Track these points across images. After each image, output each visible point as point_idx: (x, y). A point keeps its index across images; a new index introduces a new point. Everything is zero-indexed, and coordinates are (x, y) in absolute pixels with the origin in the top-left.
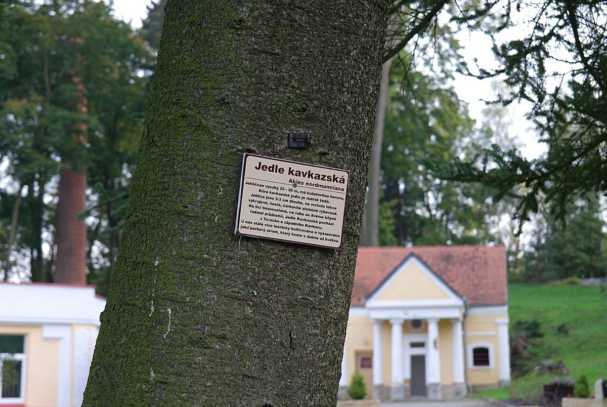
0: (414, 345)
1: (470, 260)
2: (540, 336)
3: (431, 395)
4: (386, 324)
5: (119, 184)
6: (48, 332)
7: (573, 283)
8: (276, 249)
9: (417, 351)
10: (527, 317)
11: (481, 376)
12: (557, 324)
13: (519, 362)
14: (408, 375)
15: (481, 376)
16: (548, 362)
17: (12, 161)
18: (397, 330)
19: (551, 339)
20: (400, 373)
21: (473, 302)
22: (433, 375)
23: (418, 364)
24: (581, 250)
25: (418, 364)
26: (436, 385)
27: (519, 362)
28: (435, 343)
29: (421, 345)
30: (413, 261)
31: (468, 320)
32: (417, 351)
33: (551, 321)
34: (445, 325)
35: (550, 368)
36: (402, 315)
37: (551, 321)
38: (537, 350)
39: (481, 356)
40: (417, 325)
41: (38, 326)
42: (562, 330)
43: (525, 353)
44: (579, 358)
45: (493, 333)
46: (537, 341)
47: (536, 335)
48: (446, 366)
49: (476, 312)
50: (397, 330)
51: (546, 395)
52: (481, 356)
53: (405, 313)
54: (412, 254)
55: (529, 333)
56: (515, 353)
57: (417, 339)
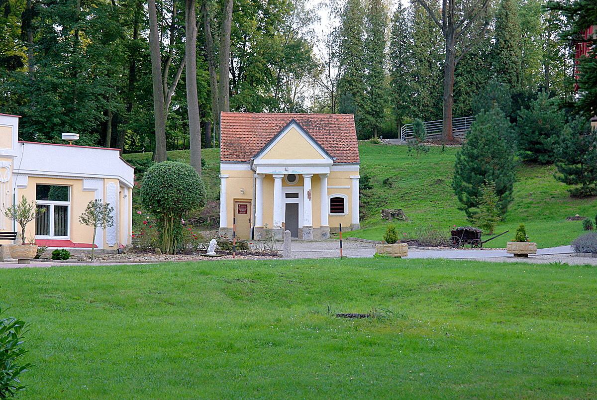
0: (288, 196)
2: (370, 188)
3: (305, 237)
6: (87, 184)
7: (375, 143)
11: (339, 219)
12: (381, 179)
18: (278, 183)
20: (279, 218)
22: (305, 219)
23: (292, 211)
24: (368, 113)
25: (292, 211)
28: (309, 194)
29: (296, 195)
30: (293, 126)
34: (317, 179)
38: (369, 200)
39: (337, 205)
40: (291, 178)
41: (80, 179)
50: (278, 183)
51: (453, 239)
52: (337, 205)
54: (293, 121)
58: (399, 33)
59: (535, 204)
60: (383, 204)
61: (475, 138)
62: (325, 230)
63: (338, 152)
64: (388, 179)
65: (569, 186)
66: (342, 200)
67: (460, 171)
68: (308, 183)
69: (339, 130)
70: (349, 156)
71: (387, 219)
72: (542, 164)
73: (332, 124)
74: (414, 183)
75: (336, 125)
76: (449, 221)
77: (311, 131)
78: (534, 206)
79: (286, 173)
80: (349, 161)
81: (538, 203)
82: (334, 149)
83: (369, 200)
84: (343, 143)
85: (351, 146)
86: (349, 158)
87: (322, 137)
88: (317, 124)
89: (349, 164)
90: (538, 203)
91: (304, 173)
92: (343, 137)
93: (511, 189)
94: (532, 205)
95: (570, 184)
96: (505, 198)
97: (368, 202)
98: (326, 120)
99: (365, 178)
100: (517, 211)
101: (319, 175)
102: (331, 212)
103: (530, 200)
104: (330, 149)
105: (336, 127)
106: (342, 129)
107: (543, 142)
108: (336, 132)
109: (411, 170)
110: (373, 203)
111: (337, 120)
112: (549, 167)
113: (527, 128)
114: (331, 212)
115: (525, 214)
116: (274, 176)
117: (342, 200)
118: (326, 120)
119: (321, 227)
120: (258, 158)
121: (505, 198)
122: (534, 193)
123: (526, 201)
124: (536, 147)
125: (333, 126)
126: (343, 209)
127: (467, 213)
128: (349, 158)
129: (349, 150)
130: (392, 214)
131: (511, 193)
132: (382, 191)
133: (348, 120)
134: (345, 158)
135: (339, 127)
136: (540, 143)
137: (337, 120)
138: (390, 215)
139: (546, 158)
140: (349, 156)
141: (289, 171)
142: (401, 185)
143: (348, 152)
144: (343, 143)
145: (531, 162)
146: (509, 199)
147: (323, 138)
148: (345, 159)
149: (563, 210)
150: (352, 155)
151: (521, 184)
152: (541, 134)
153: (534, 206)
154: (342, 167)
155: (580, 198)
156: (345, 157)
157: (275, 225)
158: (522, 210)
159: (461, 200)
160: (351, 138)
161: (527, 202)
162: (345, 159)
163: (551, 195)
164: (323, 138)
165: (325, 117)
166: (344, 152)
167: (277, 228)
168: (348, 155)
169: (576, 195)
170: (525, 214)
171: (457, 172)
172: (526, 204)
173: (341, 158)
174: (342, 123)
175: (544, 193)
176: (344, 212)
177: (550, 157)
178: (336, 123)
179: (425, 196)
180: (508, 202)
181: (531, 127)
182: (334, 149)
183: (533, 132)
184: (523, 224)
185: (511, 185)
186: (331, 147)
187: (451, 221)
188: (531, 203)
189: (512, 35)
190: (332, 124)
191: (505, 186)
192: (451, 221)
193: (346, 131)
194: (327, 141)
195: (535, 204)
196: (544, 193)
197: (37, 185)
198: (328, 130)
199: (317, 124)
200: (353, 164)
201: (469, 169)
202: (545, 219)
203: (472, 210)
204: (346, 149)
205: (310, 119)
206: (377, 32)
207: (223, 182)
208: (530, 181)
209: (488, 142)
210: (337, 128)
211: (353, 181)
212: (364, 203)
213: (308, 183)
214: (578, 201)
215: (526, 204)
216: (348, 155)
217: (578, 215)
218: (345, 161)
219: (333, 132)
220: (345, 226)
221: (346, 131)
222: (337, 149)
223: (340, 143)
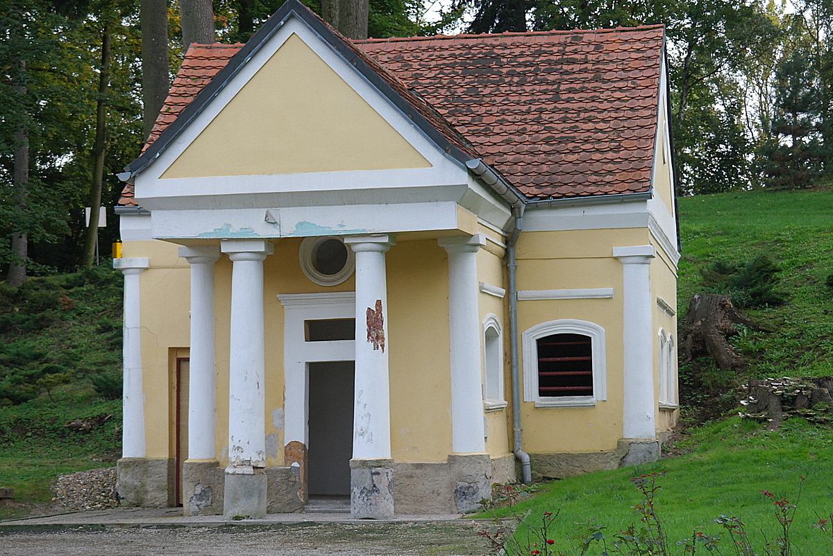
0: (317, 331)
1: (551, 67)
2: (776, 302)
4: (213, 258)
10: (741, 254)
11: (561, 428)
13: (709, 376)
14: (296, 430)
16: (786, 381)
21: (523, 190)
22: (371, 438)
25: (331, 390)
26: (374, 466)
27: (709, 376)
31: (521, 249)
33: (809, 264)
34: (420, 260)
35: (788, 402)
37: (809, 264)
38: (764, 342)
43: (728, 351)
45: (607, 290)
46: (766, 315)
47: (762, 300)
48: (437, 402)
49: (548, 222)
50: (246, 279)
52: (566, 364)
53: (269, 221)
57: (327, 310)
60: (807, 355)
63: (571, 157)
68: (369, 277)
69: (596, 79)
70: (610, 172)
71: (760, 421)
73: (574, 62)
75: (590, 66)
77: (487, 91)
79: (274, 233)
80: (607, 188)
83: (764, 342)
84: (601, 126)
85: (627, 134)
87: (525, 108)
88: (520, 65)
92: (606, 105)
97: (762, 351)
99: (758, 269)
101: (620, 259)
102: (542, 393)
104: (547, 148)
105: (586, 71)
106: (607, 76)
114: (542, 393)
116: (225, 248)
118: (555, 49)
119: (453, 459)
125: (577, 67)
128: (609, 178)
129: (616, 150)
132: (820, 311)
133: (638, 45)
135: (598, 70)
138: (774, 404)
140: (610, 172)
141: (284, 222)
143: (610, 155)
144: (601, 126)
147: (528, 112)
156: (595, 173)
157: (232, 455)
160: (636, 103)
164: (528, 112)
165: (555, 39)
166: (597, 156)
168: (610, 166)
173: (579, 178)
174: (614, 56)
176: (590, 393)
178: (590, 57)
184: (43, 313)
190: (574, 62)
193: (621, 84)
194: (538, 121)
197: (592, 395)
198: (554, 83)
199: (520, 65)
204: (604, 146)
207: (131, 287)
210: (591, 76)
212: (748, 353)
213: (369, 277)
216: (610, 166)
218: (592, 189)
219: (570, 91)
221: (621, 84)
222: (570, 146)
223: (590, 125)
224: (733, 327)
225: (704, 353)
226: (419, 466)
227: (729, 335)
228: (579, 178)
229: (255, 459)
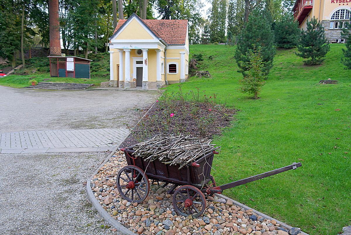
0: (138, 63)
5: (324, 59)
8: (49, 11)
9: (139, 66)
10: (198, 53)
11: (172, 77)
12: (208, 56)
13: (193, 70)
15: (172, 77)
16: (202, 71)
17: (302, 54)
19: (206, 62)
23: (139, 71)
25: (139, 71)
29: (141, 62)
31: (167, 52)
32: (139, 66)
34: (152, 53)
36: (129, 47)
42: (210, 58)
43: (195, 67)
44: (216, 69)
45: (179, 58)
47: (200, 60)
50: (127, 55)
52: (173, 68)
55: (197, 59)
56: (191, 67)
58: (231, 7)
59: (284, 69)
61: (251, 25)
62: (158, 83)
63: (174, 39)
64: (211, 56)
65: (304, 59)
66: (175, 65)
67: (240, 47)
68: (145, 55)
70: (180, 41)
72: (286, 49)
73: (175, 24)
74: (223, 58)
75: (177, 25)
76: (234, 78)
77: (163, 28)
78: (283, 70)
80: (179, 43)
81: (286, 68)
82: (173, 37)
84: (179, 34)
86: (179, 42)
89: (179, 45)
90: (286, 68)
91: (142, 48)
93: (272, 59)
94: (282, 70)
95: (305, 58)
96: (268, 65)
98: (172, 22)
100: (274, 73)
102: (169, 72)
103: (281, 67)
104: (171, 37)
106: (179, 27)
107: (287, 37)
108: (176, 29)
109: (223, 52)
110: (201, 68)
111: (179, 22)
112: (290, 50)
113: (280, 30)
114: (169, 72)
115: (279, 75)
116: (124, 50)
117: (175, 65)
118: (172, 22)
119: (157, 81)
120: (113, 38)
121: (268, 65)
122: (283, 63)
123: (278, 67)
124: (284, 40)
125: (175, 25)
126: (176, 71)
127: (243, 74)
128: (179, 42)
129: (181, 38)
130: (202, 74)
131: (272, 62)
133: (184, 23)
134: (177, 42)
136: (286, 38)
137: (179, 22)
138: (201, 74)
139: (289, 45)
140: (180, 41)
142: (217, 59)
143: (180, 38)
144: (179, 34)
145: (281, 48)
146: (270, 66)
148: (177, 42)
149: (302, 73)
150: (182, 40)
151: (276, 58)
152: (287, 34)
153: (283, 70)
154: (175, 46)
155: (310, 66)
157: (126, 80)
158: (277, 72)
159: (239, 66)
161: (279, 68)
162: (177, 42)
163: (293, 64)
166: (178, 38)
167: (127, 82)
168: (180, 40)
169: (307, 64)
170: (279, 75)
171: (238, 48)
172: (279, 69)
173: (175, 42)
174: (181, 24)
175: (289, 63)
176: (176, 72)
177: (290, 45)
179: (226, 64)
180: (269, 67)
181: (282, 30)
182: (173, 37)
183: (283, 33)
185: (272, 56)
186: (171, 36)
187: (235, 78)
188: (282, 68)
189: (271, 8)
190: (175, 24)
191: (268, 57)
192: (235, 78)
194: (170, 33)
195: (284, 69)
196: (289, 63)
200: (181, 45)
201: (245, 46)
202: (292, 78)
203: (247, 72)
205: (164, 22)
206: (223, 8)
207: (111, 55)
208: (280, 57)
209: (259, 28)
211: (182, 55)
212: (198, 67)
213: (145, 55)
214: (309, 68)
215: (279, 69)
217: (330, 79)
218: (177, 43)
219: (174, 29)
220: (177, 80)
223: (177, 34)
224: (196, 63)
225: (192, 67)
226: (152, 82)
227: (195, 65)
228: (175, 42)
229: (129, 81)
